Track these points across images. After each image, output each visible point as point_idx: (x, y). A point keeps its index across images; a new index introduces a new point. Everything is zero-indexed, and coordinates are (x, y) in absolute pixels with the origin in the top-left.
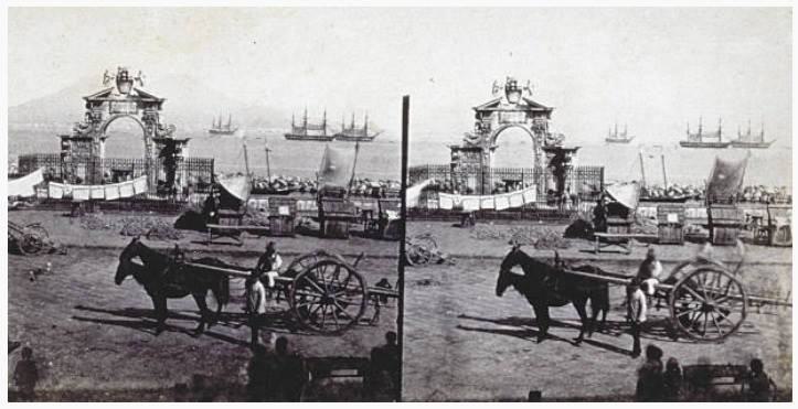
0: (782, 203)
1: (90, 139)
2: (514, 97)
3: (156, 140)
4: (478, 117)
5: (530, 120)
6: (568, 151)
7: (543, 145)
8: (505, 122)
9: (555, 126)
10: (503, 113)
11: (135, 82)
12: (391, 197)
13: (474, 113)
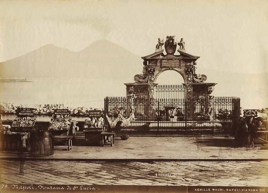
4: (145, 63)
13: (143, 60)
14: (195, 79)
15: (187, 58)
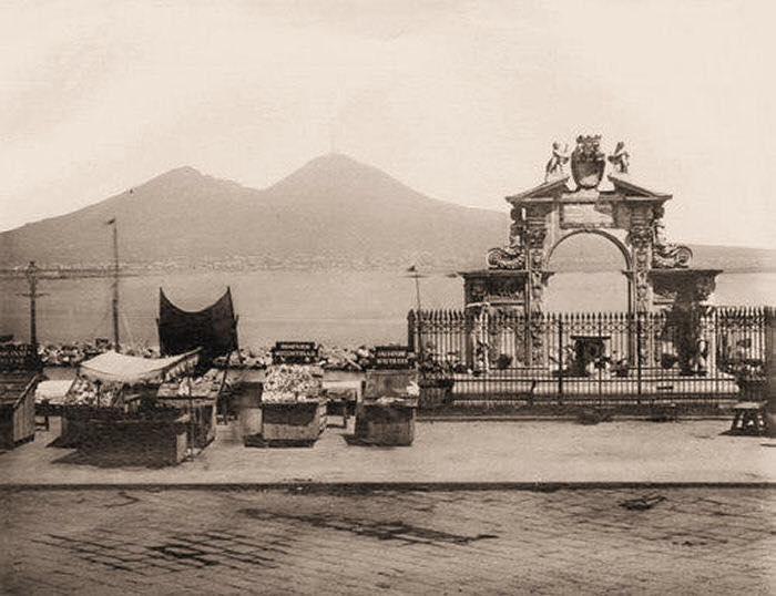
9: (672, 230)
14: (657, 258)
15: (635, 198)
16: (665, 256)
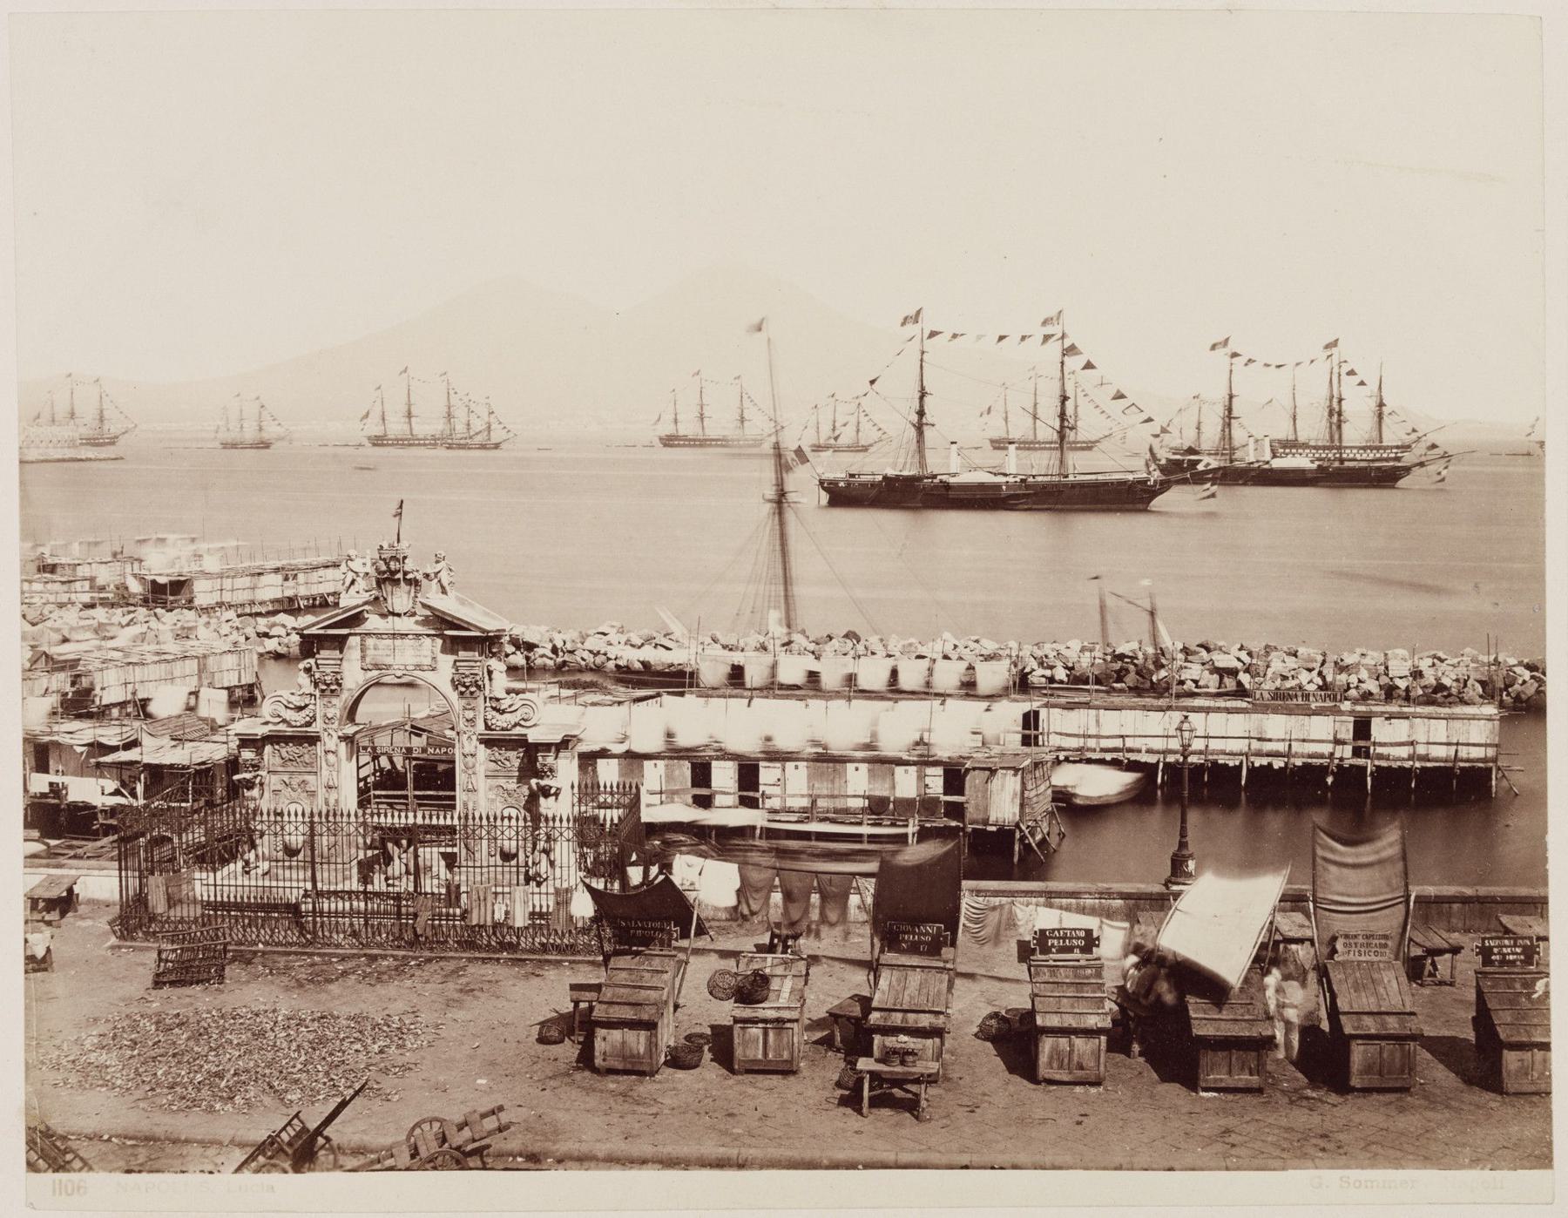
0: (1070, 950)
1: (313, 740)
2: (400, 599)
3: (489, 743)
5: (446, 661)
6: (547, 747)
7: (480, 727)
8: (377, 667)
10: (370, 642)
11: (424, 582)
12: (1062, 950)
16: (503, 712)
